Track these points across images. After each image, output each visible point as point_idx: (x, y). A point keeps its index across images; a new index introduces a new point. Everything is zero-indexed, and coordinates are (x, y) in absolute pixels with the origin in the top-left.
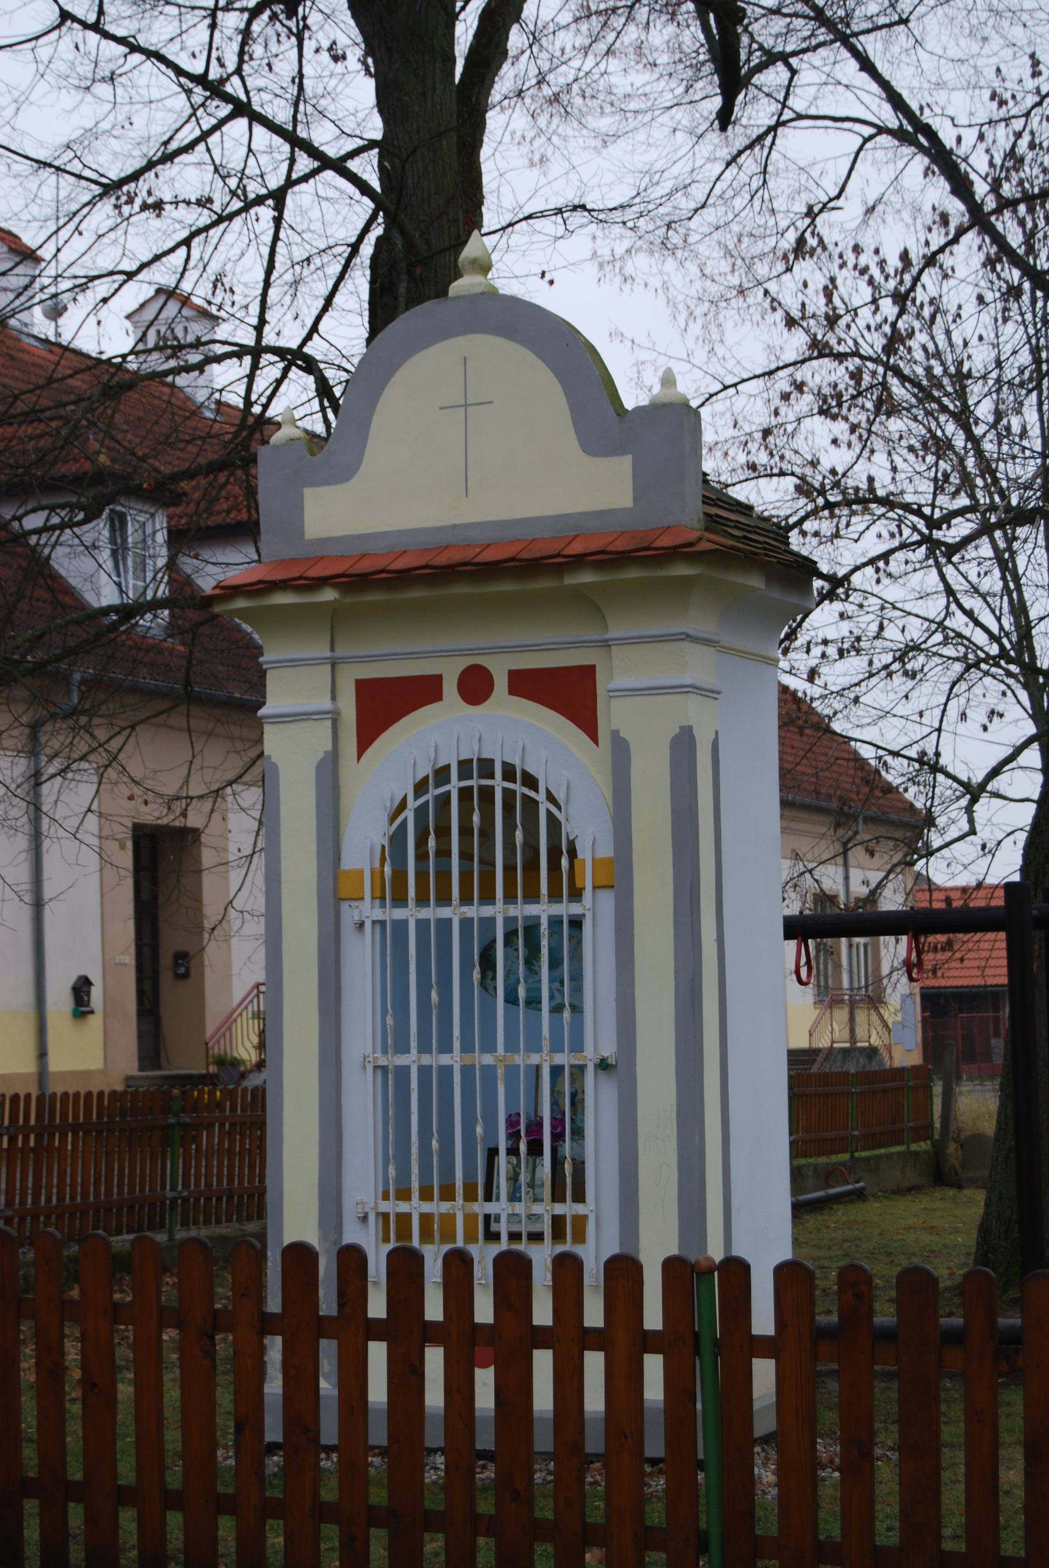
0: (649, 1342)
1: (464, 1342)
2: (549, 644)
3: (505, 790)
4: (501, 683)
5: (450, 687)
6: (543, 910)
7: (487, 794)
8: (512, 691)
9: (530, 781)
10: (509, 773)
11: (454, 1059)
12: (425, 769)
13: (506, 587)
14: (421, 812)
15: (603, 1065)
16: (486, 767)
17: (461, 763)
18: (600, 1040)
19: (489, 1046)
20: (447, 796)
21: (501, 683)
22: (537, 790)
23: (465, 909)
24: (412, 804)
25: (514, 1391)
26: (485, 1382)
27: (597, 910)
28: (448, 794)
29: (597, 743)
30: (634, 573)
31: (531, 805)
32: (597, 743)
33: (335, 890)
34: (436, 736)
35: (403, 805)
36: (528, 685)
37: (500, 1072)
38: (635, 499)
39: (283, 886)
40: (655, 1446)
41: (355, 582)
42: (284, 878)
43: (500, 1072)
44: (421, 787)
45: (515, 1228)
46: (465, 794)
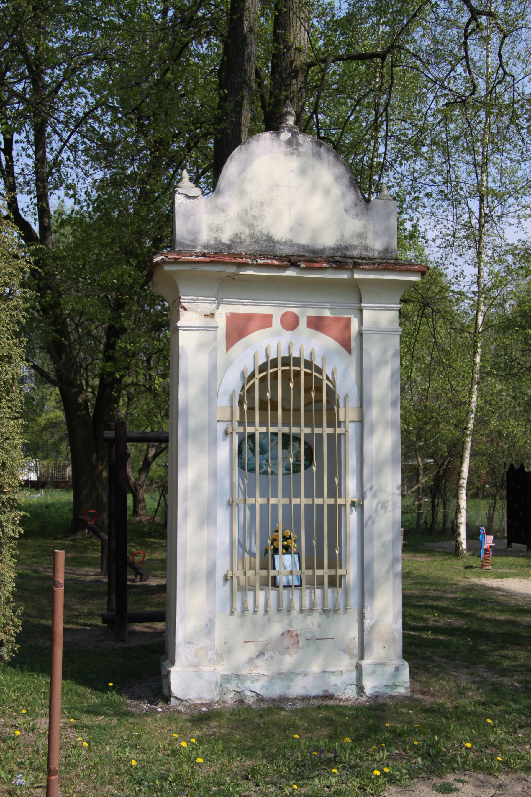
4: (303, 322)
5: (276, 322)
7: (297, 374)
9: (319, 371)
10: (309, 364)
12: (262, 360)
14: (263, 380)
15: (353, 504)
16: (297, 361)
17: (284, 358)
19: (298, 496)
20: (276, 373)
24: (258, 376)
29: (227, 351)
31: (319, 382)
32: (227, 351)
35: (253, 375)
44: (263, 368)
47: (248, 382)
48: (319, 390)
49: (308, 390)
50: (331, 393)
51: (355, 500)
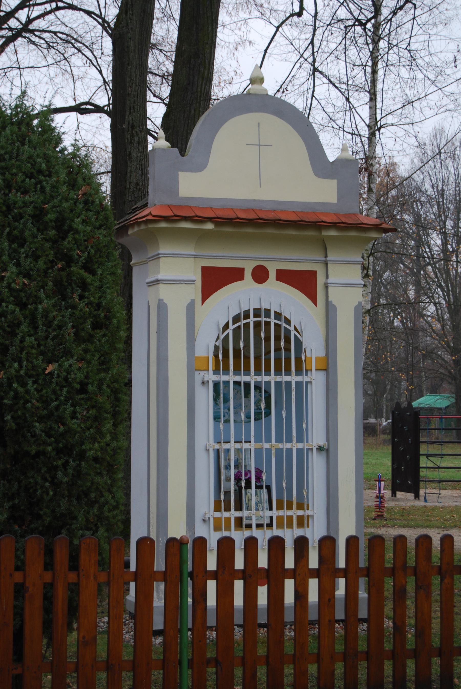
0: (214, 575)
1: (251, 575)
2: (299, 259)
3: (275, 324)
4: (272, 275)
5: (248, 274)
6: (293, 379)
7: (268, 324)
8: (278, 279)
9: (288, 321)
10: (278, 315)
11: (253, 446)
12: (234, 312)
13: (291, 232)
14: (236, 331)
15: (320, 449)
16: (267, 312)
18: (317, 437)
19: (268, 440)
21: (272, 275)
22: (290, 325)
23: (256, 377)
24: (232, 327)
25: (276, 596)
26: (262, 594)
27: (317, 380)
28: (249, 323)
29: (316, 306)
30: (353, 234)
31: (288, 332)
32: (316, 306)
33: (194, 365)
34: (240, 296)
35: (226, 326)
36: (284, 276)
37: (273, 452)
38: (338, 200)
39: (169, 362)
40: (340, 614)
41: (220, 221)
42: (170, 359)
43: (273, 452)
44: (236, 319)
45: (260, 522)
46: (257, 325)
47: (223, 332)
48: (288, 340)
49: (277, 338)
50: (299, 343)
51: (321, 444)
